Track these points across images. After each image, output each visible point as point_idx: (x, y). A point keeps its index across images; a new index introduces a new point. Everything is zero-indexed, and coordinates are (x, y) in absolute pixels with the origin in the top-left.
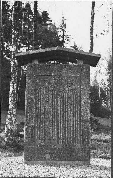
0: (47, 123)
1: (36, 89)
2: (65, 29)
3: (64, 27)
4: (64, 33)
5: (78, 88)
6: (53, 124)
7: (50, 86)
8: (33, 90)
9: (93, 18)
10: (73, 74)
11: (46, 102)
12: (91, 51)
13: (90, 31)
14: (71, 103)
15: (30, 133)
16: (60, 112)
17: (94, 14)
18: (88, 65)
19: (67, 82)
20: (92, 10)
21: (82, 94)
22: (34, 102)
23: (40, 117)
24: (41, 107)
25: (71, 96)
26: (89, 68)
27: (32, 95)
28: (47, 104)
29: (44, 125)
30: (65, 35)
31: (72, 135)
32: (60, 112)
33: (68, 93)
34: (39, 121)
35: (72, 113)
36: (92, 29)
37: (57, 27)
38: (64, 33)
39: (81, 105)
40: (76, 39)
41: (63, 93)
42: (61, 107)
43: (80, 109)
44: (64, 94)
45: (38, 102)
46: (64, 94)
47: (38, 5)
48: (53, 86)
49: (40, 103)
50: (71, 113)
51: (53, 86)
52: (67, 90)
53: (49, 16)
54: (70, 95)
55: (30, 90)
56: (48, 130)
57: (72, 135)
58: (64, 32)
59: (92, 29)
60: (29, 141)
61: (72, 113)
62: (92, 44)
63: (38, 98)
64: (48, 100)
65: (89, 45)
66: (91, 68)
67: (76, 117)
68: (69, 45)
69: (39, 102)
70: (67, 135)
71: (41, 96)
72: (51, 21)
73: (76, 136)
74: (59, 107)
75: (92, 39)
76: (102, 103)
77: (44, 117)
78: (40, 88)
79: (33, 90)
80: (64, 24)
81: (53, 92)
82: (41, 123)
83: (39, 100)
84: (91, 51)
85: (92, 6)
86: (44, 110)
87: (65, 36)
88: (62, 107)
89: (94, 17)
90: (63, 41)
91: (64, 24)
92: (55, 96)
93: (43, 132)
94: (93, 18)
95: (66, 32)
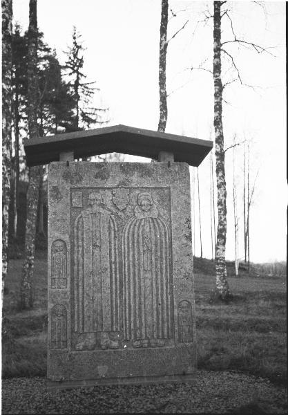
0: (100, 295)
1: (72, 219)
2: (80, 70)
3: (76, 64)
4: (78, 78)
5: (165, 215)
6: (112, 297)
7: (102, 211)
8: (64, 220)
9: (163, 52)
10: (154, 183)
11: (95, 245)
12: (162, 125)
13: (157, 81)
14: (152, 248)
15: (61, 318)
16: (126, 268)
17: (166, 45)
18: (185, 164)
19: (141, 203)
20: (161, 37)
21: (173, 228)
22: (69, 248)
23: (83, 281)
24: (85, 259)
25: (150, 231)
26: (187, 169)
27: (64, 233)
28: (96, 251)
29: (93, 300)
30: (80, 82)
31: (155, 320)
32: (126, 268)
33: (144, 225)
34: (81, 291)
35: (154, 270)
36: (162, 78)
37: (62, 63)
38: (78, 78)
39: (174, 252)
40: (115, 97)
41: (132, 227)
42: (128, 259)
43: (171, 260)
44: (134, 229)
45: (78, 247)
46: (134, 229)
47: (38, 20)
48: (110, 210)
49: (83, 251)
50: (151, 270)
51: (110, 210)
52: (141, 219)
53: (44, 40)
54: (148, 230)
55: (58, 220)
56: (101, 310)
57: (155, 320)
58: (80, 76)
59: (162, 78)
60: (59, 338)
61: (154, 270)
62: (164, 107)
63: (78, 238)
64: (100, 243)
65: (158, 112)
66: (191, 168)
67: (162, 278)
68: (90, 106)
69: (81, 249)
70: (145, 320)
71: (83, 234)
72: (48, 50)
73: (163, 322)
74: (125, 259)
75: (163, 98)
76: (26, 230)
77: (91, 281)
78: (81, 217)
79: (64, 220)
80: (79, 56)
81: (109, 227)
82: (85, 295)
83: (80, 243)
84: (162, 125)
85: (161, 28)
86: (91, 266)
87: (81, 85)
88: (131, 259)
89: (167, 51)
90: (78, 97)
91: (79, 56)
92: (115, 234)
93: (89, 317)
94: (163, 52)
95: (82, 75)
